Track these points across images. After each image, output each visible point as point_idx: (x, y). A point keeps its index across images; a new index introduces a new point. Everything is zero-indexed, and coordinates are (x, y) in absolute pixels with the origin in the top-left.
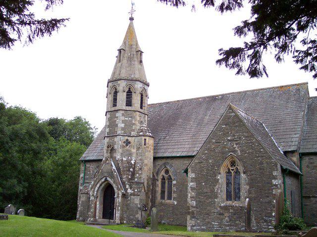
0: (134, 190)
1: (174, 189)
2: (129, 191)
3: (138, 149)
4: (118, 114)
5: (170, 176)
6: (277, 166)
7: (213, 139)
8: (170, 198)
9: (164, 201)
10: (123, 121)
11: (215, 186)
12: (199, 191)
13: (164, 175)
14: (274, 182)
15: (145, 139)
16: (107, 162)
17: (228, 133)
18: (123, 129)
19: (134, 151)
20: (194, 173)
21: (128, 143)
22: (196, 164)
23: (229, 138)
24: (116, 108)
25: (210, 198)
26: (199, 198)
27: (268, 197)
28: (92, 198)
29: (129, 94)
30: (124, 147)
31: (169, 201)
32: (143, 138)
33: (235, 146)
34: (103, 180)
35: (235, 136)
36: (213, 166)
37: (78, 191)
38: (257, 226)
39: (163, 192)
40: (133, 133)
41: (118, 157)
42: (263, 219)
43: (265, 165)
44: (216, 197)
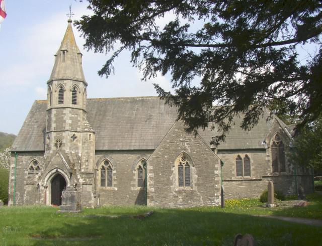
0: (84, 180)
1: (114, 177)
2: (81, 181)
3: (84, 143)
4: (65, 111)
5: (109, 166)
6: (218, 161)
7: (167, 139)
8: (110, 184)
9: (104, 188)
10: (70, 117)
11: (170, 176)
12: (157, 181)
13: (104, 165)
14: (216, 172)
15: (90, 135)
16: (57, 155)
17: (180, 135)
18: (70, 125)
19: (80, 145)
20: (152, 165)
21: (74, 137)
22: (153, 159)
23: (181, 139)
24: (62, 105)
25: (167, 185)
26: (157, 185)
27: (211, 183)
28: (41, 188)
29: (62, 91)
30: (72, 141)
31: (109, 188)
32: (89, 133)
33: (186, 145)
34: (55, 170)
35: (185, 138)
36: (168, 161)
37: (9, 181)
38: (204, 204)
39: (103, 181)
40: (78, 129)
41: (67, 151)
42: (208, 198)
43: (209, 160)
44: (172, 184)
